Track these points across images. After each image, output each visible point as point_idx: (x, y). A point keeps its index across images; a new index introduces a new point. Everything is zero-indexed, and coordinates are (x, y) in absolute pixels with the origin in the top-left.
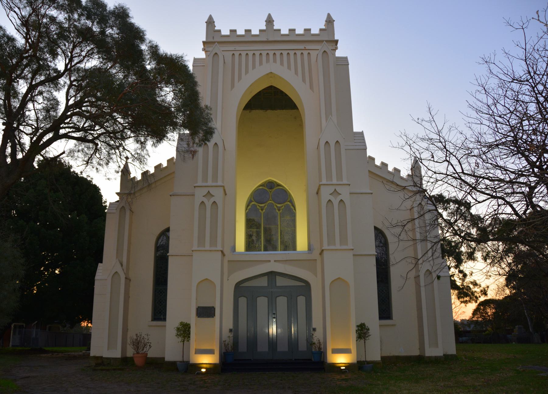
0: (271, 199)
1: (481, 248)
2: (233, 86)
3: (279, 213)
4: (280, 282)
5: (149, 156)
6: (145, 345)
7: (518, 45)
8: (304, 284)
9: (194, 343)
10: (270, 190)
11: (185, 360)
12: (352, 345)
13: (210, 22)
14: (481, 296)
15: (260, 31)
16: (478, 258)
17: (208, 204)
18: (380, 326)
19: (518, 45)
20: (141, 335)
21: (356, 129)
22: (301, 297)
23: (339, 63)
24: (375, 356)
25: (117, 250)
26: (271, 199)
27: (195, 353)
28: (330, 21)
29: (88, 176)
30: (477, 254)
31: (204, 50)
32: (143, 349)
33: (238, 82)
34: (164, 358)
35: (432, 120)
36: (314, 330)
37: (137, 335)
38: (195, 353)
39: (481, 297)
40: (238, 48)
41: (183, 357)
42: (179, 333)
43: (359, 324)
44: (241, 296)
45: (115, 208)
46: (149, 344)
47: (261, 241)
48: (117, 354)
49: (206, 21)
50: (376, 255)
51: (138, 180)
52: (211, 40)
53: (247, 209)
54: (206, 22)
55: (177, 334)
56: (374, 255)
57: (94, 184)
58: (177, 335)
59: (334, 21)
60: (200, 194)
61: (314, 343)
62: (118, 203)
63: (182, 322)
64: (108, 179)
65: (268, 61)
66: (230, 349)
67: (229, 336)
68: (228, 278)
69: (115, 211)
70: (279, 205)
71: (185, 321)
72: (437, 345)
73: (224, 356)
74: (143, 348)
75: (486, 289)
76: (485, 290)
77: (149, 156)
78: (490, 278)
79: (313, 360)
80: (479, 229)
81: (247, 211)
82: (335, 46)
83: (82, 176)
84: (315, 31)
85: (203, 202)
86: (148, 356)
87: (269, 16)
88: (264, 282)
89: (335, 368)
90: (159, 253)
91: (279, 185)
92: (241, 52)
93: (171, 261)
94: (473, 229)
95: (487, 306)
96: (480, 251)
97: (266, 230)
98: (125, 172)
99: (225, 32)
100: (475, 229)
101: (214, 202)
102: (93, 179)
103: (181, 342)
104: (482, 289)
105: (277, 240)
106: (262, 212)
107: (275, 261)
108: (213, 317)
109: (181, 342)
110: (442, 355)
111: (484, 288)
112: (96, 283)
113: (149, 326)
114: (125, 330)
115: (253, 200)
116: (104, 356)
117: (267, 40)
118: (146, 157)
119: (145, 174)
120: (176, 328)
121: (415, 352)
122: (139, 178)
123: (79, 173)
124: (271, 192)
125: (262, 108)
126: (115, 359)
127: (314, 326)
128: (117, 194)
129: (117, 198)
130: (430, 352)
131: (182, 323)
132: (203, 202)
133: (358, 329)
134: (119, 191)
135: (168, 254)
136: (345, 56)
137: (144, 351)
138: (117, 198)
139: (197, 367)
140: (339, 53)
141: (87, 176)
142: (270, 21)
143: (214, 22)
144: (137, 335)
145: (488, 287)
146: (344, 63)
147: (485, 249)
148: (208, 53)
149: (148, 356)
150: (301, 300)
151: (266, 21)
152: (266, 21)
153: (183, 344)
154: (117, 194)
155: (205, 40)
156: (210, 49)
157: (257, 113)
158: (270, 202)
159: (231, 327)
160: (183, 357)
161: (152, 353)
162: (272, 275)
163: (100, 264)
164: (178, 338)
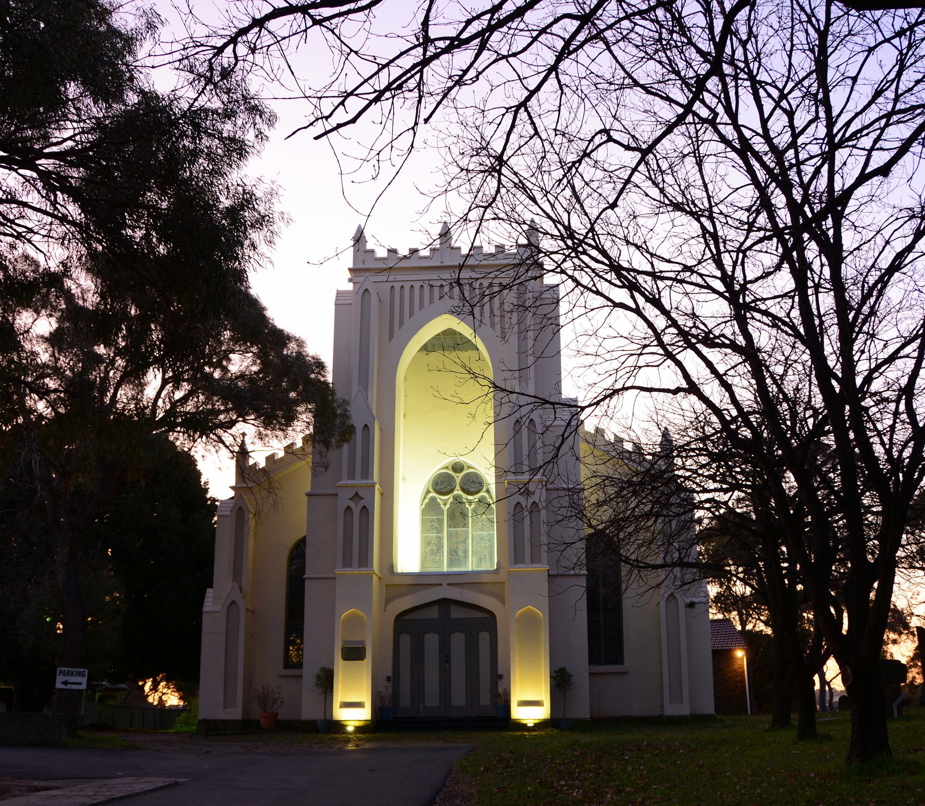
0: (458, 487)
2: (391, 336)
4: (456, 613)
6: (275, 701)
8: (488, 616)
9: (340, 695)
10: (458, 475)
11: (328, 718)
12: (544, 695)
13: (359, 238)
17: (356, 509)
18: (590, 674)
20: (269, 688)
22: (457, 634)
24: (581, 710)
25: (234, 570)
26: (458, 487)
27: (340, 707)
32: (272, 707)
36: (501, 677)
37: (263, 687)
38: (340, 707)
40: (399, 278)
41: (325, 713)
43: (557, 669)
44: (430, 632)
45: (229, 509)
47: (443, 552)
48: (236, 713)
51: (261, 467)
52: (361, 266)
53: (425, 498)
58: (317, 685)
60: (344, 501)
62: (232, 501)
66: (387, 702)
69: (229, 513)
70: (470, 497)
71: (327, 666)
72: (681, 701)
73: (377, 709)
81: (423, 506)
85: (349, 507)
86: (279, 718)
88: (434, 613)
89: (522, 727)
90: (293, 567)
91: (469, 467)
92: (404, 284)
93: (308, 584)
97: (450, 535)
98: (242, 454)
101: (364, 507)
105: (466, 551)
106: (445, 509)
107: (448, 584)
108: (363, 660)
110: (688, 713)
112: (205, 618)
113: (280, 676)
114: (249, 682)
115: (431, 489)
116: (218, 718)
117: (440, 264)
119: (270, 459)
121: (656, 712)
122: (262, 464)
124: (458, 477)
126: (235, 722)
127: (499, 673)
128: (232, 488)
129: (232, 493)
130: (671, 710)
131: (322, 669)
132: (349, 507)
133: (558, 676)
134: (233, 484)
135: (304, 576)
138: (232, 493)
139: (339, 726)
144: (263, 687)
148: (358, 285)
149: (279, 718)
150: (484, 637)
154: (232, 488)
155: (351, 266)
156: (361, 279)
157: (436, 357)
158: (457, 492)
159: (390, 673)
160: (325, 713)
161: (284, 714)
162: (444, 603)
163: (209, 590)
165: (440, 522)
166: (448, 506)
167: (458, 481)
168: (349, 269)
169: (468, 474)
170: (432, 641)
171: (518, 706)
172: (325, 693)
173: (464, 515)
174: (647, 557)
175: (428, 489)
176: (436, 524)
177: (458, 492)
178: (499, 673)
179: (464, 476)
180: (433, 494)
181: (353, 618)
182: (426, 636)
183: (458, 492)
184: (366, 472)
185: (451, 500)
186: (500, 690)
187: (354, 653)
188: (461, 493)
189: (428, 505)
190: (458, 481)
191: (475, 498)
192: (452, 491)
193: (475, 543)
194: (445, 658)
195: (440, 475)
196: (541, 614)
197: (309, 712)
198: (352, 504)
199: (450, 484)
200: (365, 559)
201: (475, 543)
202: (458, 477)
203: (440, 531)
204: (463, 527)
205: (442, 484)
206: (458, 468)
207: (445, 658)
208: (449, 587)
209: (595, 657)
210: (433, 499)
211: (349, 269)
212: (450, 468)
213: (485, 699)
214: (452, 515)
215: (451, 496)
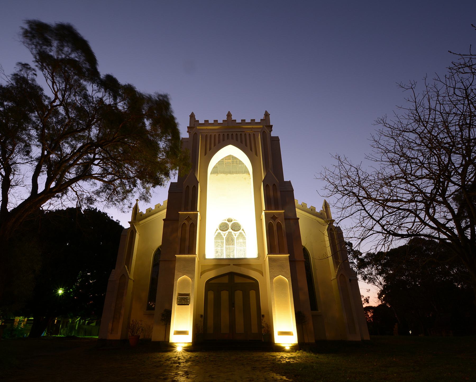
0: (230, 228)
1: (360, 272)
3: (235, 237)
4: (238, 280)
5: (151, 197)
7: (409, 100)
10: (230, 223)
11: (166, 340)
13: (192, 116)
14: (364, 303)
15: (223, 121)
16: (359, 278)
19: (409, 100)
21: (285, 179)
23: (273, 140)
26: (230, 228)
28: (267, 115)
29: (117, 220)
30: (358, 276)
31: (188, 132)
33: (210, 150)
34: (151, 340)
35: (342, 165)
36: (263, 316)
39: (365, 304)
42: (163, 318)
46: (142, 328)
49: (190, 115)
50: (305, 261)
54: (190, 116)
55: (162, 319)
56: (303, 261)
57: (120, 225)
59: (270, 114)
61: (263, 327)
63: (166, 309)
64: (124, 212)
65: (228, 138)
67: (200, 321)
68: (201, 276)
74: (137, 331)
75: (368, 298)
76: (367, 299)
77: (151, 197)
78: (369, 291)
79: (263, 341)
80: (358, 259)
82: (271, 129)
83: (112, 219)
84: (258, 120)
87: (229, 112)
88: (225, 280)
94: (355, 259)
95: (368, 311)
96: (360, 274)
97: (227, 249)
98: (136, 208)
99: (201, 121)
100: (356, 260)
102: (120, 222)
103: (164, 325)
104: (365, 298)
106: (224, 237)
109: (164, 325)
111: (366, 298)
115: (218, 229)
118: (150, 197)
120: (161, 314)
122: (144, 212)
123: (110, 217)
125: (224, 173)
128: (129, 222)
136: (277, 136)
137: (137, 334)
140: (273, 134)
141: (117, 220)
142: (229, 115)
143: (195, 116)
145: (369, 297)
146: (276, 140)
147: (363, 273)
150: (252, 293)
151: (227, 115)
152: (227, 115)
153: (166, 327)
154: (129, 222)
164: (162, 322)
165: (222, 243)
166: (226, 236)
167: (230, 226)
168: (188, 127)
169: (234, 223)
170: (225, 295)
171: (278, 335)
172: (166, 325)
173: (233, 240)
174: (432, 233)
175: (217, 229)
176: (220, 244)
177: (230, 230)
178: (262, 313)
179: (233, 224)
180: (219, 231)
181: (184, 281)
182: (222, 292)
183: (230, 230)
184: (195, 209)
185: (227, 233)
186: (263, 325)
187: (184, 301)
188: (231, 230)
189: (217, 235)
190: (230, 226)
191: (237, 233)
192: (227, 229)
193: (238, 252)
194: (232, 304)
195: (222, 223)
196: (287, 280)
197: (156, 336)
198: (186, 222)
199: (226, 227)
200: (191, 250)
201: (238, 252)
202: (230, 224)
203: (222, 247)
204: (232, 245)
205: (224, 227)
206: (229, 220)
207: (232, 304)
208: (235, 266)
209: (312, 309)
210: (219, 233)
211: (188, 127)
212: (227, 220)
213: (255, 329)
214: (227, 240)
215: (227, 232)
